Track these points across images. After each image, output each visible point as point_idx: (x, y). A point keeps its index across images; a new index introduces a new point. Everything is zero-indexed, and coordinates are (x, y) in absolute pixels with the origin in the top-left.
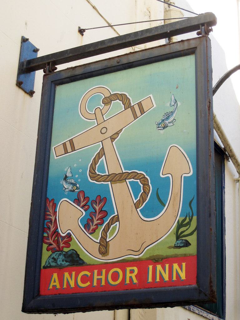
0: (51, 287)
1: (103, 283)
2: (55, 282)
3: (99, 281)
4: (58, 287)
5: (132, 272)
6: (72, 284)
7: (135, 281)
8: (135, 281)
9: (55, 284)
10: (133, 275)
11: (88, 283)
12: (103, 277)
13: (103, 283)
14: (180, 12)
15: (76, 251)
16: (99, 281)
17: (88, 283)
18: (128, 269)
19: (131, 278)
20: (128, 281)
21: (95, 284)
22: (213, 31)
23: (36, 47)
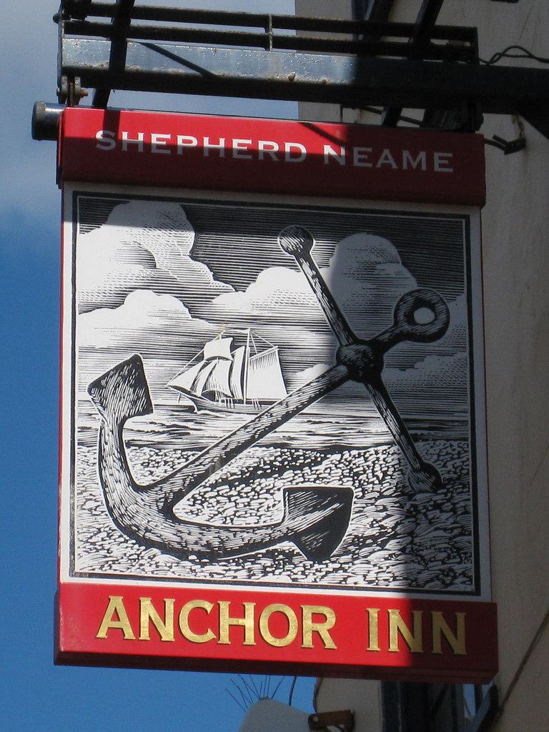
0: (102, 634)
1: (250, 638)
2: (116, 617)
3: (237, 632)
4: (394, 166)
5: (319, 618)
6: (167, 633)
7: (329, 643)
8: (329, 643)
9: (116, 625)
10: (324, 629)
11: (210, 635)
12: (248, 622)
13: (250, 638)
14: (257, 414)
15: (496, 55)
16: (237, 632)
17: (210, 635)
18: (308, 611)
19: (316, 634)
20: (308, 641)
21: (225, 638)
22: (506, 156)
23: (110, 224)
